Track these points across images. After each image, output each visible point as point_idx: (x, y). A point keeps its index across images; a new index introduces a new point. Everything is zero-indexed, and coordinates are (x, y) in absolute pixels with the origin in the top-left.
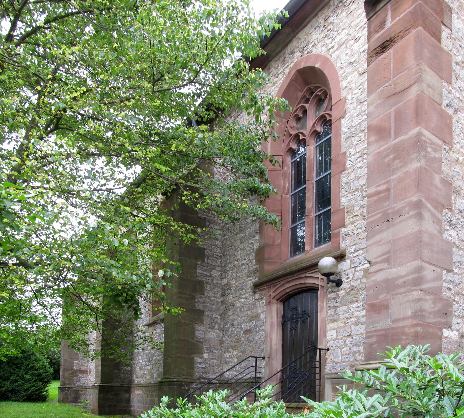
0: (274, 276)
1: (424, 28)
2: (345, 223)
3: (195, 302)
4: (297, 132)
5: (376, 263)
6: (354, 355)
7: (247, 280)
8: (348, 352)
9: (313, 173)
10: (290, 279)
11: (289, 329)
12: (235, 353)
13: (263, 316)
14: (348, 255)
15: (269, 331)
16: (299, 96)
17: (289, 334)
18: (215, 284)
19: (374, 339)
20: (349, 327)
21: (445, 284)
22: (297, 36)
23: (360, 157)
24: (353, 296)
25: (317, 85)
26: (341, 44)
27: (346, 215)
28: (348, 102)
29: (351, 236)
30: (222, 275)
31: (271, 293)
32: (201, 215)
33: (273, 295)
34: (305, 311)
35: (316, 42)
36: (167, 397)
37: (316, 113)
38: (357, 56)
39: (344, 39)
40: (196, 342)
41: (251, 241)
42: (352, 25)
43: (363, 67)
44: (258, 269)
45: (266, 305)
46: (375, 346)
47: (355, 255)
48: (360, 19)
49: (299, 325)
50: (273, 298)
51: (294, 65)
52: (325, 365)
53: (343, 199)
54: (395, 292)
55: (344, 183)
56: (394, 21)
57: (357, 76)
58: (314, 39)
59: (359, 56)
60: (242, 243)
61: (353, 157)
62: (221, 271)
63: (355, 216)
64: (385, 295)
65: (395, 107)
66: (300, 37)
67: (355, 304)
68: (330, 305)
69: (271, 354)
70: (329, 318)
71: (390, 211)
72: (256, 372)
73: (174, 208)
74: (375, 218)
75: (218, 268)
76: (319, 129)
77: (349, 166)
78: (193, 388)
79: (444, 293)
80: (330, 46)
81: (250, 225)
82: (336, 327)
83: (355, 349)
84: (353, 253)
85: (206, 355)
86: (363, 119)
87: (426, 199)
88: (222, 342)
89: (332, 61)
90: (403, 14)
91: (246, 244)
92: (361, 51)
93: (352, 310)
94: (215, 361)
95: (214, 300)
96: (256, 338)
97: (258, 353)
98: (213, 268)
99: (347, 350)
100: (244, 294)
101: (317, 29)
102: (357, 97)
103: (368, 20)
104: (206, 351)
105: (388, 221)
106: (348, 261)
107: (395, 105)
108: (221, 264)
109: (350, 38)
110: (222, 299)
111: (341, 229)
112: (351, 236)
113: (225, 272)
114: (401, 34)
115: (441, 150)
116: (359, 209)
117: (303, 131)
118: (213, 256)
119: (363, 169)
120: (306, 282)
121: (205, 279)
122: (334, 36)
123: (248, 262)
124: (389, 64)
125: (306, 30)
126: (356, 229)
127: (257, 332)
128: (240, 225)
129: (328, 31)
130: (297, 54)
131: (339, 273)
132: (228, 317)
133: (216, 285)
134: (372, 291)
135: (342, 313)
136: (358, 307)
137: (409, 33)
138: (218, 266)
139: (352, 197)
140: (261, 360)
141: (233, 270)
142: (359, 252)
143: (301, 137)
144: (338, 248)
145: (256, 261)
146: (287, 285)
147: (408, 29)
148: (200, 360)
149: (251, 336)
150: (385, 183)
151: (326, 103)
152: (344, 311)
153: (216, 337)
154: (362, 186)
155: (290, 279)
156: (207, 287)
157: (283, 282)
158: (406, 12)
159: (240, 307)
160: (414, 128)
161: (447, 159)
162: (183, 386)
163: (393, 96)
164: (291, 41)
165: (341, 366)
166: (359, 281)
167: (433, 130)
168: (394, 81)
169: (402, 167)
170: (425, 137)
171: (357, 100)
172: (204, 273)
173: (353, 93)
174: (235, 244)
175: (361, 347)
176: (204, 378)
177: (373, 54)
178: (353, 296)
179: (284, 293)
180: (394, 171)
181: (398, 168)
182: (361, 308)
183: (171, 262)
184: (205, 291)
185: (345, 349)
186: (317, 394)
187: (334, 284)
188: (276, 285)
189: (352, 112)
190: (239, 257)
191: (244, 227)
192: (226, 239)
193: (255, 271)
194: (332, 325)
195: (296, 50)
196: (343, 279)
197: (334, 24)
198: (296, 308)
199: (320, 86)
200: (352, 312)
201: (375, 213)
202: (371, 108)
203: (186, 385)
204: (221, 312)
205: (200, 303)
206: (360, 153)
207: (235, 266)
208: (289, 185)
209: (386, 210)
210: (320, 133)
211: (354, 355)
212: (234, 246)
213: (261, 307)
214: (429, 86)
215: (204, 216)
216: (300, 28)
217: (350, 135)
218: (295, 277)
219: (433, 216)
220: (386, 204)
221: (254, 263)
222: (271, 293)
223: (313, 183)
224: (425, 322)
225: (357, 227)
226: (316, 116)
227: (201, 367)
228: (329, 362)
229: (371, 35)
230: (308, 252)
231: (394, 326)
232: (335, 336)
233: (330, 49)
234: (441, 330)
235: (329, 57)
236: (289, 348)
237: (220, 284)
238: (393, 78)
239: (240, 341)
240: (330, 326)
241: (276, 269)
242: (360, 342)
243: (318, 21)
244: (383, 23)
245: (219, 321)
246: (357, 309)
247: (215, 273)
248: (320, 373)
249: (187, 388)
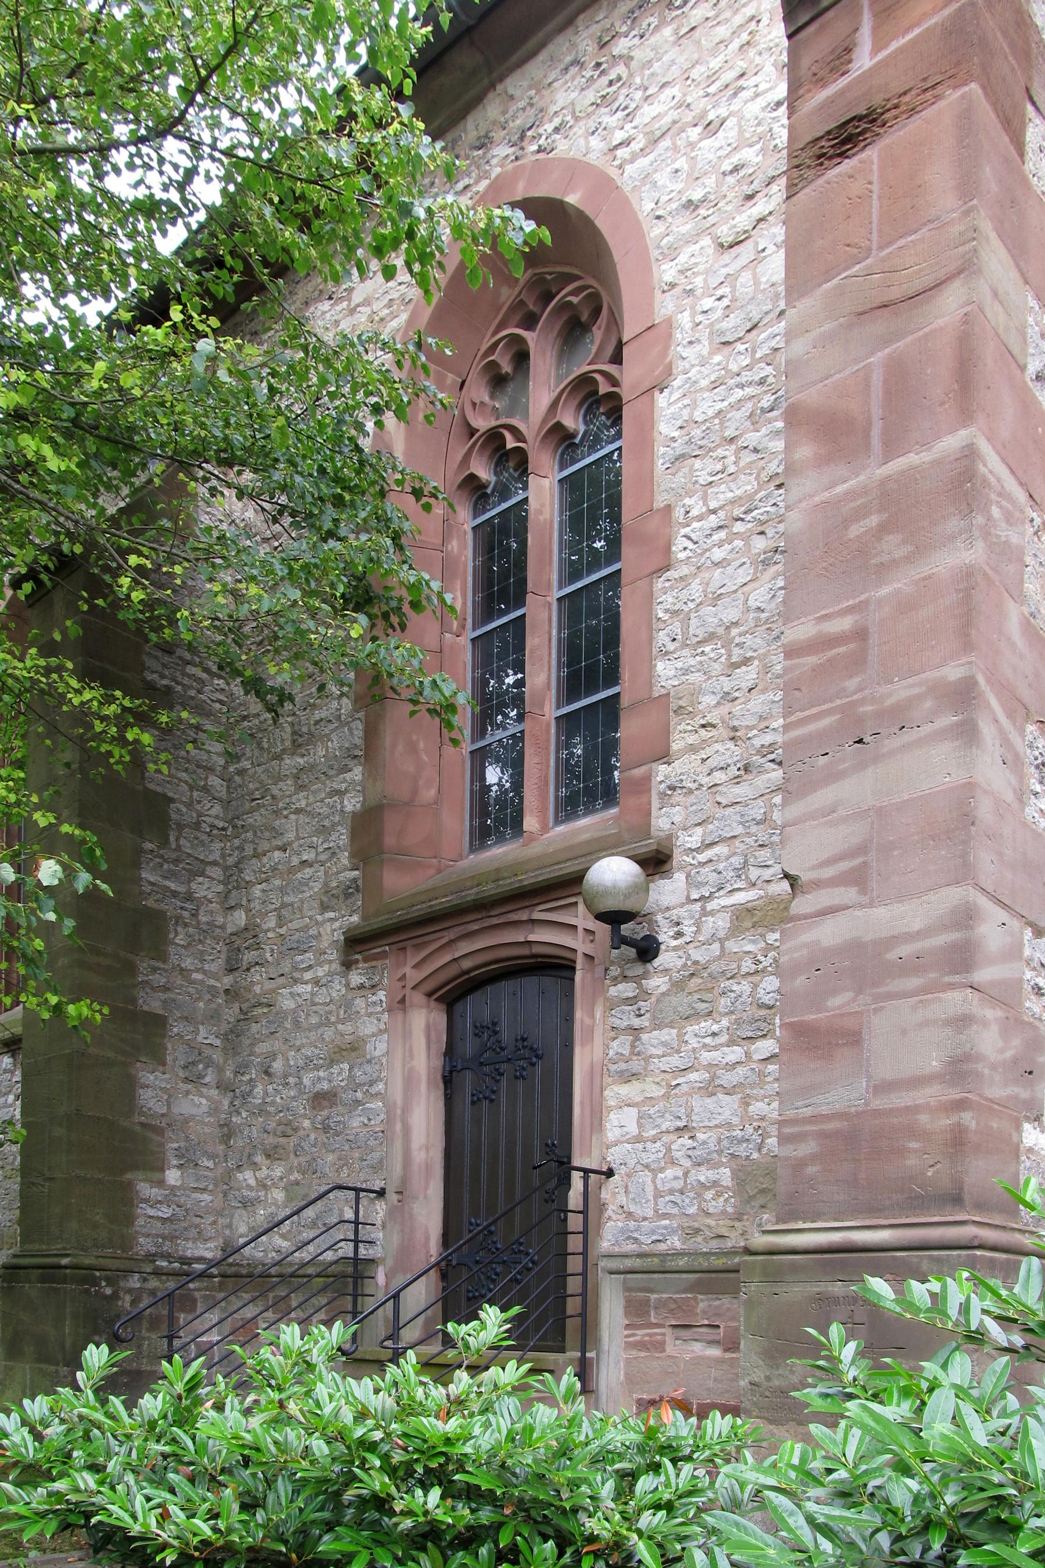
0: (419, 910)
1: (983, 88)
2: (668, 746)
3: (135, 986)
4: (494, 423)
5: (818, 884)
6: (699, 1195)
7: (319, 918)
8: (678, 1185)
9: (551, 571)
10: (475, 927)
11: (468, 1099)
12: (278, 1171)
13: (378, 1048)
14: (678, 857)
15: (399, 1102)
16: (503, 298)
17: (468, 1115)
18: (204, 927)
19: (807, 1148)
20: (682, 1101)
21: (1029, 975)
22: (500, 88)
23: (720, 527)
24: (696, 996)
25: (567, 269)
26: (658, 133)
27: (674, 719)
28: (679, 336)
29: (691, 791)
30: (227, 895)
31: (408, 970)
32: (155, 676)
33: (414, 976)
34: (524, 1039)
35: (568, 118)
36: (104, 1348)
37: (559, 366)
38: (711, 181)
39: (667, 120)
40: (138, 1129)
41: (335, 786)
42: (695, 74)
43: (734, 223)
44: (360, 883)
45: (390, 1010)
46: (811, 1170)
47: (702, 857)
48: (721, 58)
49: (504, 1083)
50: (413, 988)
51: (490, 186)
52: (599, 1227)
53: (660, 666)
54: (882, 990)
55: (667, 611)
56: (880, 56)
57: (711, 251)
58: (560, 104)
59: (719, 184)
60: (302, 788)
61: (695, 525)
62: (225, 883)
63: (703, 726)
64: (849, 995)
65: (887, 351)
66: (511, 91)
67: (703, 1024)
68: (617, 1022)
69: (405, 1180)
70: (613, 1068)
71: (869, 708)
72: (356, 1242)
73: (64, 632)
74: (812, 727)
75: (216, 872)
76: (572, 420)
77: (682, 556)
78: (130, 1291)
79: (1027, 1004)
80: (619, 136)
81: (333, 726)
82: (639, 1099)
83: (704, 1175)
84: (697, 850)
85: (173, 1176)
86: (732, 399)
87: (989, 681)
88: (227, 1132)
89: (627, 189)
90: (917, 31)
91: (314, 793)
92: (727, 166)
93: (694, 1043)
94: (206, 1197)
95: (202, 981)
96: (355, 1123)
97: (362, 1176)
98: (199, 868)
99: (676, 1178)
100: (310, 967)
101: (573, 70)
102: (711, 325)
103: (790, 37)
104: (175, 1162)
105: (860, 741)
106: (680, 877)
107: (887, 342)
108: (223, 856)
109: (689, 116)
110: (227, 981)
111: (654, 765)
112: (691, 791)
113: (237, 888)
114: (906, 99)
115: (1023, 523)
116: (718, 703)
117: (514, 422)
118: (197, 826)
119: (730, 570)
120: (532, 938)
121: (170, 906)
122: (633, 105)
123: (323, 857)
124: (864, 198)
125: (534, 69)
126: (705, 769)
127: (358, 1102)
128: (292, 724)
129: (611, 83)
130: (502, 151)
131: (647, 917)
132: (252, 1045)
133: (208, 931)
134: (801, 981)
135: (660, 1052)
136: (714, 1034)
137: (938, 98)
138: (215, 863)
139: (692, 662)
140: (372, 1200)
141: (266, 881)
142: (717, 850)
143: (511, 443)
144: (645, 830)
145: (352, 856)
146: (466, 947)
147: (933, 87)
148: (155, 1193)
149: (337, 1114)
150: (850, 610)
151: (598, 333)
152: (664, 1044)
153: (210, 1115)
154: (728, 628)
155: (475, 927)
156: (177, 934)
157: (450, 935)
158: (925, 26)
159: (294, 1011)
160: (952, 431)
161: (1035, 555)
162: (95, 1282)
163: (878, 312)
164: (478, 100)
165: (653, 1232)
166: (716, 946)
167: (1004, 447)
168: (883, 260)
169: (908, 559)
170: (985, 465)
171: (711, 333)
172: (167, 883)
173: (699, 309)
174: (275, 791)
175: (722, 1170)
176: (167, 1256)
177: (807, 158)
178: (696, 996)
179: (453, 971)
180: (883, 570)
181: (894, 563)
182: (724, 1038)
183: (66, 828)
184: (172, 950)
185: (669, 1173)
186: (572, 1325)
187: (632, 952)
188: (425, 944)
189: (694, 370)
190: (291, 836)
191: (310, 733)
192: (241, 772)
193: (348, 891)
194: (625, 1090)
195: (498, 135)
196: (661, 938)
197: (633, 64)
198: (493, 1028)
199: (576, 272)
200: (694, 1050)
201: (814, 711)
202: (799, 347)
203: (108, 1279)
204: (224, 1027)
205: (153, 988)
206: (722, 514)
207: (274, 869)
208: (464, 603)
209: (854, 704)
210: (573, 436)
211: (699, 1195)
212: (273, 797)
213: (370, 1015)
214: (996, 295)
215: (165, 682)
216: (514, 58)
217: (687, 450)
218: (495, 921)
219: (1006, 742)
220: (852, 684)
221: (346, 862)
222: (408, 970)
223: (550, 604)
224: (980, 1095)
225: (711, 763)
226: (559, 379)
227: (158, 1218)
228: (614, 1217)
229: (801, 92)
230: (532, 837)
231: (878, 1103)
232: (633, 1129)
233: (616, 147)
234: (1018, 1128)
235: (613, 173)
236: (467, 1161)
237: (223, 927)
238: (881, 248)
239: (296, 1130)
240: (615, 1092)
241: (423, 887)
242: (720, 1152)
243: (574, 45)
244: (846, 52)
245: (217, 1056)
246: (708, 1040)
247: (204, 888)
248: (585, 1254)
249: (108, 1291)
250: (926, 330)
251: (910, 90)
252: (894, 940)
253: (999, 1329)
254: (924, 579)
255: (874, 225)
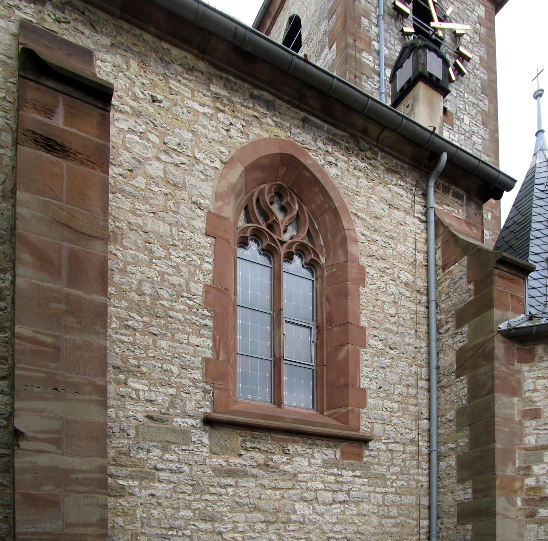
54: (69, 488)
90: (84, 135)
105: (56, 389)
163: (66, 227)
250: (88, 250)
251: (82, 154)
252: (74, 471)
253: (503, 351)
254: (86, 341)
255: (64, 191)
